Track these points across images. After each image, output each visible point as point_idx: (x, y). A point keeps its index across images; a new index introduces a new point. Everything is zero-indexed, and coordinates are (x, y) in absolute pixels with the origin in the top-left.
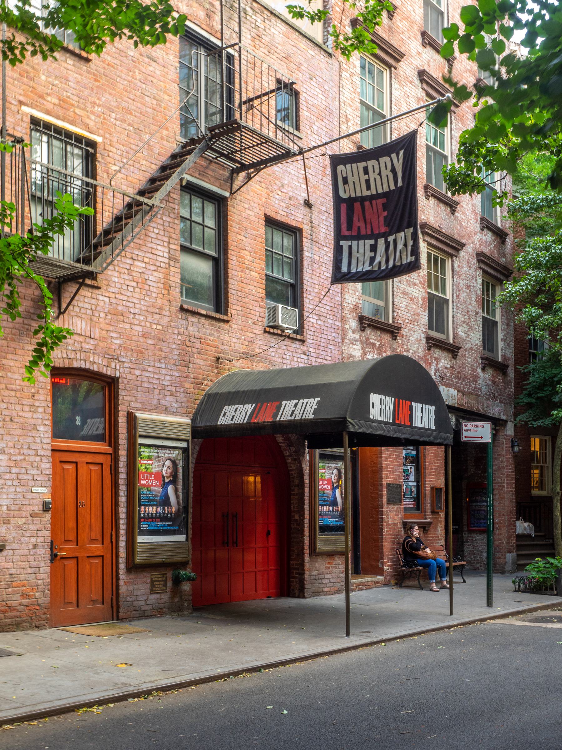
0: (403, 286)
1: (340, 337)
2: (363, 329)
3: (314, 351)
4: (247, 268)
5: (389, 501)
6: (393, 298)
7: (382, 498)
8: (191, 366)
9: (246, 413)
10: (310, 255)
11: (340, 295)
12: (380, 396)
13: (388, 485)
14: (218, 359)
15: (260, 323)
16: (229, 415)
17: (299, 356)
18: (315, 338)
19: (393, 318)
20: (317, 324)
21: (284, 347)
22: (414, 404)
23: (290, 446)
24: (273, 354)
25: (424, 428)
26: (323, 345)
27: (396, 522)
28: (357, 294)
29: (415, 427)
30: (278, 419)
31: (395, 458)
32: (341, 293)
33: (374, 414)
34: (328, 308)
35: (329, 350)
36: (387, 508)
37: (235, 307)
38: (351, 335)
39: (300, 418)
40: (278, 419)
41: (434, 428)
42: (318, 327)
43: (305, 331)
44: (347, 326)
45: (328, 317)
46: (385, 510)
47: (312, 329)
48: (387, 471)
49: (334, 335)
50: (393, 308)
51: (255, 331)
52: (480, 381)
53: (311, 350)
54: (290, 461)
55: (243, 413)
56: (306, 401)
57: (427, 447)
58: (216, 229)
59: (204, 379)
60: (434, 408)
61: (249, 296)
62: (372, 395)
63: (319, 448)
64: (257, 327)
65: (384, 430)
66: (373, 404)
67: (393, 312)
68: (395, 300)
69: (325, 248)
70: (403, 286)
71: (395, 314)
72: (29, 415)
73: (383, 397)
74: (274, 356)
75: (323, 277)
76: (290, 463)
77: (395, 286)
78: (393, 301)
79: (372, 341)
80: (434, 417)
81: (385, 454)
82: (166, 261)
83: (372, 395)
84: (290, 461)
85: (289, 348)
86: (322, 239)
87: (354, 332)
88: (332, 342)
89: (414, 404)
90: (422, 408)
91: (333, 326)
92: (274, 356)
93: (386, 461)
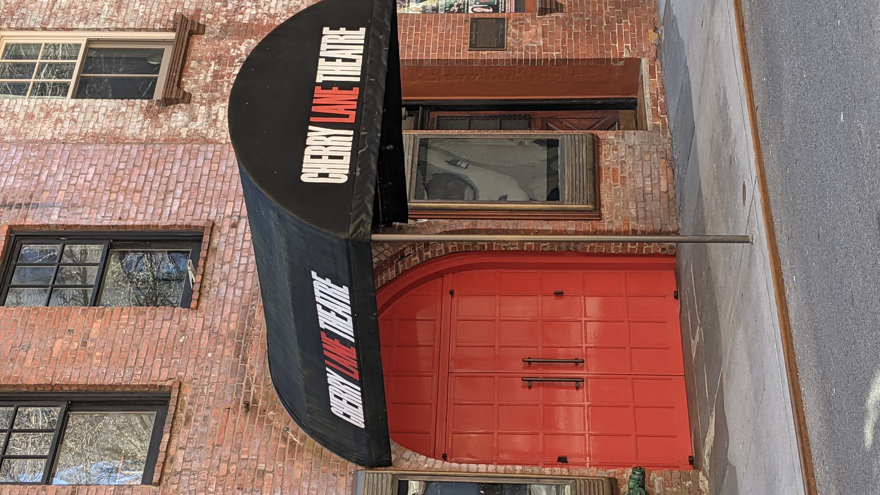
0: (106, 8)
1: (203, 148)
2: (187, 98)
3: (231, 204)
4: (84, 344)
5: (501, 45)
6: (129, 29)
7: (496, 61)
8: (262, 466)
9: (343, 384)
10: (56, 211)
11: (127, 147)
12: (307, 159)
13: (473, 46)
14: (247, 405)
15: (184, 319)
16: (349, 409)
17: (240, 238)
18: (208, 203)
19: (165, 30)
20: (181, 198)
21: (226, 267)
22: (320, 79)
23: (403, 256)
24: (238, 292)
25: (365, 55)
26: (219, 184)
27: (540, 30)
28: (123, 109)
29: (362, 76)
30: (353, 340)
31: (423, 30)
32: (124, 144)
33: (339, 173)
34: (151, 172)
35: (229, 171)
36: (514, 50)
37: (156, 373)
38: (200, 124)
39: (349, 308)
40: (353, 340)
41: (363, 30)
42: (187, 194)
43: (195, 223)
44: (184, 132)
45: (167, 173)
46: (517, 55)
47: (191, 208)
48: (446, 51)
49: (201, 161)
50: (147, 30)
51: (198, 330)
53: (229, 212)
54: (429, 253)
55: (344, 388)
56: (317, 293)
57: (405, 54)
58: (16, 404)
59: (285, 439)
60: (326, 30)
61: (136, 341)
62: (304, 178)
63: (405, 201)
64: (191, 325)
65: (368, 150)
66: (321, 175)
67: (154, 30)
68: (132, 25)
69: (43, 178)
70: (106, 8)
71: (158, 26)
73: (308, 152)
74: (243, 289)
75: (95, 182)
76: (433, 252)
77: (107, 25)
78: (135, 30)
79: (209, 79)
80: (343, 30)
81: (415, 53)
83: (304, 178)
84: (429, 253)
85: (227, 259)
86: (26, 184)
87: (194, 119)
88: (215, 166)
90: (328, 59)
91: (185, 163)
92: (243, 289)
93: (428, 52)
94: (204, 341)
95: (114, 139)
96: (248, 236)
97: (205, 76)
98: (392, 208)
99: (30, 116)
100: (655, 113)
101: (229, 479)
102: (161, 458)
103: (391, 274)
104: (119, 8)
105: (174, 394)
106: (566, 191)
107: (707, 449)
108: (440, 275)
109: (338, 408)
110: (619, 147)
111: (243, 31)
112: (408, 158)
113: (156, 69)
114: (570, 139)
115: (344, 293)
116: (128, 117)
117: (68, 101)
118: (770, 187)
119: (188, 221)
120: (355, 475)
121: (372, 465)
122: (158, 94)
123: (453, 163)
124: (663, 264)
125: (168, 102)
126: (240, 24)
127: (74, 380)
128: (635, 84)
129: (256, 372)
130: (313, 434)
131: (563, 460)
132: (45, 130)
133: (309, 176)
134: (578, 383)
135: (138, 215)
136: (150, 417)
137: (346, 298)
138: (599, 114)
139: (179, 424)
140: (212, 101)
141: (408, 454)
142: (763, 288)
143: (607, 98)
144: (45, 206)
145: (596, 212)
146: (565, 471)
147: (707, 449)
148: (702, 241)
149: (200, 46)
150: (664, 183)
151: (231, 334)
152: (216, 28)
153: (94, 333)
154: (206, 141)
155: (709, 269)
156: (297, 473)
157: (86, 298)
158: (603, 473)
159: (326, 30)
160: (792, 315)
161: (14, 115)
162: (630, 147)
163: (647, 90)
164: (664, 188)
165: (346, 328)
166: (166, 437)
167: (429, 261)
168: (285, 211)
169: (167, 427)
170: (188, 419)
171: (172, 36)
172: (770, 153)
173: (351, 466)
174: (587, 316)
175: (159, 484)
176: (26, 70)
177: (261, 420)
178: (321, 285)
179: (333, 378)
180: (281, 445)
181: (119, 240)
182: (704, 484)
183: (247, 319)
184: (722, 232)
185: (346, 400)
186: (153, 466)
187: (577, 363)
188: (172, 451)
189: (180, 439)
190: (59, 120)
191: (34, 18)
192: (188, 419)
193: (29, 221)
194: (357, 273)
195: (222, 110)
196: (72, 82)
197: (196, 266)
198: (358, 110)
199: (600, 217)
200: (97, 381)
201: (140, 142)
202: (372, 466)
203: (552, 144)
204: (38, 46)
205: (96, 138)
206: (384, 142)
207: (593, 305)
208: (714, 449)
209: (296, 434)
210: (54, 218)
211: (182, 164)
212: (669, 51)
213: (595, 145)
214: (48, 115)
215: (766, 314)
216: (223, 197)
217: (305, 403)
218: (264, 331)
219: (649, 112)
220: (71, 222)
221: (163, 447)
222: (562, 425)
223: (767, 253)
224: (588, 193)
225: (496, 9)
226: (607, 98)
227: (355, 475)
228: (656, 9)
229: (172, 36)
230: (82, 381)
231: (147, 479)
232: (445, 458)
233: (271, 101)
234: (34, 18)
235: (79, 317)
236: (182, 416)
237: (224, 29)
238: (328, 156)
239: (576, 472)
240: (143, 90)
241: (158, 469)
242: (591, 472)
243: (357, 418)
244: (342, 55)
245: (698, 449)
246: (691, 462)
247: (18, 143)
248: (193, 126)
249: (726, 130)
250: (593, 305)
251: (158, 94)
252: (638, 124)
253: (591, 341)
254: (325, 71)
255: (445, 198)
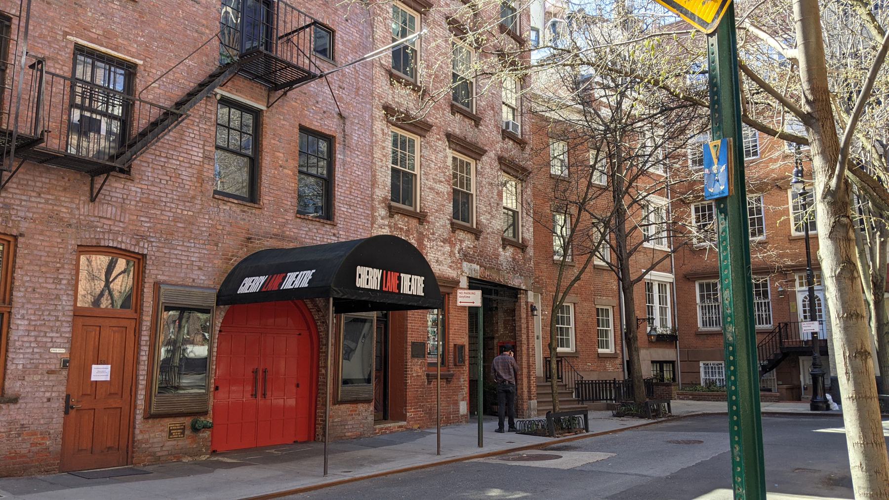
2: (391, 216)
5: (413, 356)
8: (220, 245)
12: (367, 269)
13: (413, 343)
14: (250, 239)
16: (247, 286)
22: (402, 275)
25: (412, 295)
33: (360, 283)
37: (267, 198)
38: (380, 221)
44: (376, 214)
52: (501, 258)
57: (410, 313)
60: (423, 278)
62: (359, 267)
72: (53, 286)
73: (370, 269)
82: (201, 159)
83: (359, 267)
87: (382, 219)
89: (402, 275)
94: (280, 220)
95: (374, 183)
96: (329, 241)
97: (401, 224)
98: (342, 307)
99: (384, 148)
100: (382, 429)
101: (214, 230)
102: (225, 199)
103: (310, 306)
104: (429, 188)
105: (256, 206)
106: (348, 388)
107: (221, 459)
108: (309, 328)
109: (247, 281)
110: (367, 412)
111: (420, 240)
112: (364, 314)
113: (404, 203)
114: (371, 389)
115: (305, 284)
116: (383, 189)
117: (390, 165)
118: (350, 484)
119: (337, 214)
120: (214, 289)
121: (219, 296)
122: (393, 204)
123: (364, 337)
124: (310, 434)
125: (390, 208)
126: (423, 240)
127: (264, 161)
128: (396, 419)
129: (266, 243)
130: (235, 269)
131: (217, 388)
132: (378, 154)
133: (360, 270)
134: (254, 395)
135: (340, 193)
136: (245, 192)
137: (302, 285)
138: (382, 403)
139: (242, 208)
140: (390, 227)
141: (223, 314)
142: (302, 482)
143: (389, 405)
144: (344, 152)
145: (336, 402)
146: (212, 389)
147: (221, 459)
148: (325, 453)
149: (414, 222)
150: (349, 434)
151: (284, 232)
152: (422, 230)
153: (286, 171)
154: (372, 224)
155: (250, 465)
156: (216, 261)
157: (302, 166)
158: (210, 408)
159: (423, 278)
160: (291, 496)
161: (384, 141)
162: (170, 434)
163: (392, 425)
164: (347, 434)
165: (287, 285)
166: (236, 201)
167: (316, 324)
168: (344, 258)
169: (240, 202)
170: (244, 212)
171: (418, 211)
172: (366, 483)
173: (218, 287)
174: (287, 400)
175: (214, 197)
176: (403, 148)
177: (242, 245)
178: (308, 274)
179: (263, 279)
180: (230, 254)
181: (328, 184)
182: (203, 458)
183: (291, 239)
184: (329, 462)
185: (252, 285)
186: (221, 195)
187: (264, 395)
188: (229, 204)
189: (234, 207)
190: (382, 160)
191: (426, 153)
192: (244, 212)
193: (337, 145)
194: (313, 291)
195: (386, 231)
196: (398, 167)
197: (317, 217)
198: (388, 292)
199: (334, 404)
200: (263, 171)
201: (372, 195)
202: (218, 296)
203: (368, 381)
204: (414, 153)
205: (374, 176)
206: (372, 302)
207: (292, 402)
208: (221, 462)
209: (235, 261)
210: (339, 156)
211: (362, 214)
212: (410, 434)
213: (367, 401)
214: (384, 156)
215: (290, 484)
216: (347, 230)
217: (251, 264)
218: (285, 247)
219: (382, 426)
220: (337, 163)
221: (231, 200)
222: (233, 388)
223: (320, 483)
224: (346, 399)
225: (429, 354)
226: (389, 405)
227: (214, 289)
228: (429, 428)
229: (418, 211)
230: (263, 164)
231: (216, 192)
232: (220, 331)
233: (397, 255)
234: (426, 153)
235: (293, 164)
236: (246, 209)
237: (421, 233)
238: (368, 278)
239: (211, 395)
240: (395, 196)
241: (221, 197)
242: (211, 401)
243: (242, 290)
244: (412, 285)
245: (222, 454)
246: (214, 451)
247: (372, 142)
248: (379, 218)
249: (376, 462)
250: (292, 402)
251: (393, 204)
252: (377, 421)
253: (274, 402)
254: (405, 277)
255: (345, 331)
